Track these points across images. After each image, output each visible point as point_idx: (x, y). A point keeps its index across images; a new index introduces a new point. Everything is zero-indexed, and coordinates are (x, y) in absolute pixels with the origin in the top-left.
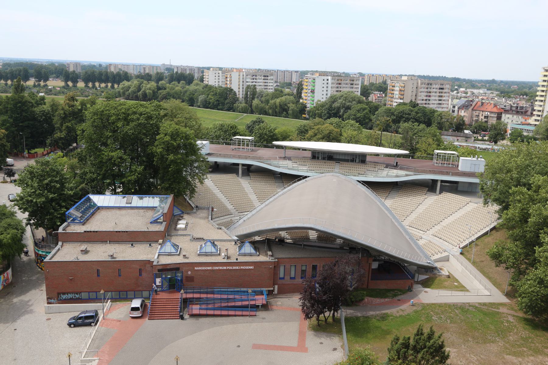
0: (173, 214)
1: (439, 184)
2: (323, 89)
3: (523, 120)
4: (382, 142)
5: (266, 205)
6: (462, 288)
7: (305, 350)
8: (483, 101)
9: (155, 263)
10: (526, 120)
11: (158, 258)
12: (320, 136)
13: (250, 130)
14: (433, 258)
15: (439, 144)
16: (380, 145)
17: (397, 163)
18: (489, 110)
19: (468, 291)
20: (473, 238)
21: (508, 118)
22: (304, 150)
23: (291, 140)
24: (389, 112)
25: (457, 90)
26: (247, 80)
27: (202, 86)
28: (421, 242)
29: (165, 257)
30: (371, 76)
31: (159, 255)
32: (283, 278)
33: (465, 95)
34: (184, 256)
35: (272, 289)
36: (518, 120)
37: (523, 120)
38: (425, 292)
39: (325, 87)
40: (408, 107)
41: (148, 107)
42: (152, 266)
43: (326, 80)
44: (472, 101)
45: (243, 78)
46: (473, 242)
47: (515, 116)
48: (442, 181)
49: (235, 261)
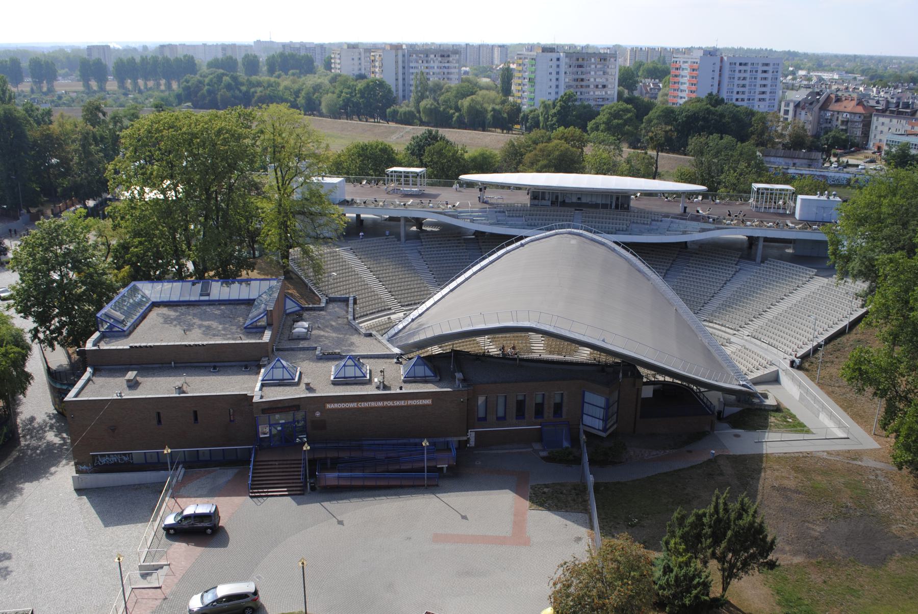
0: (285, 311)
1: (761, 244)
2: (550, 77)
3: (908, 128)
4: (659, 170)
5: (452, 291)
6: (798, 427)
7: (527, 542)
8: (840, 94)
9: (255, 400)
10: (913, 128)
11: (261, 389)
12: (543, 162)
13: (417, 153)
14: (751, 376)
15: (762, 173)
16: (654, 175)
17: (685, 208)
18: (849, 110)
19: (808, 432)
20: (821, 339)
21: (883, 124)
22: (518, 188)
23: (495, 171)
24: (669, 115)
25: (793, 73)
26: (411, 65)
27: (329, 77)
28: (729, 350)
29: (272, 388)
30: (635, 51)
31: (263, 385)
32: (485, 419)
33: (806, 83)
34: (308, 384)
35: (465, 438)
36: (899, 127)
37: (908, 128)
38: (737, 436)
39: (554, 73)
40: (704, 105)
41: (227, 119)
42: (252, 404)
43: (555, 60)
44: (818, 94)
45: (403, 62)
46: (819, 346)
47: (895, 121)
48: (766, 240)
49: (399, 391)
